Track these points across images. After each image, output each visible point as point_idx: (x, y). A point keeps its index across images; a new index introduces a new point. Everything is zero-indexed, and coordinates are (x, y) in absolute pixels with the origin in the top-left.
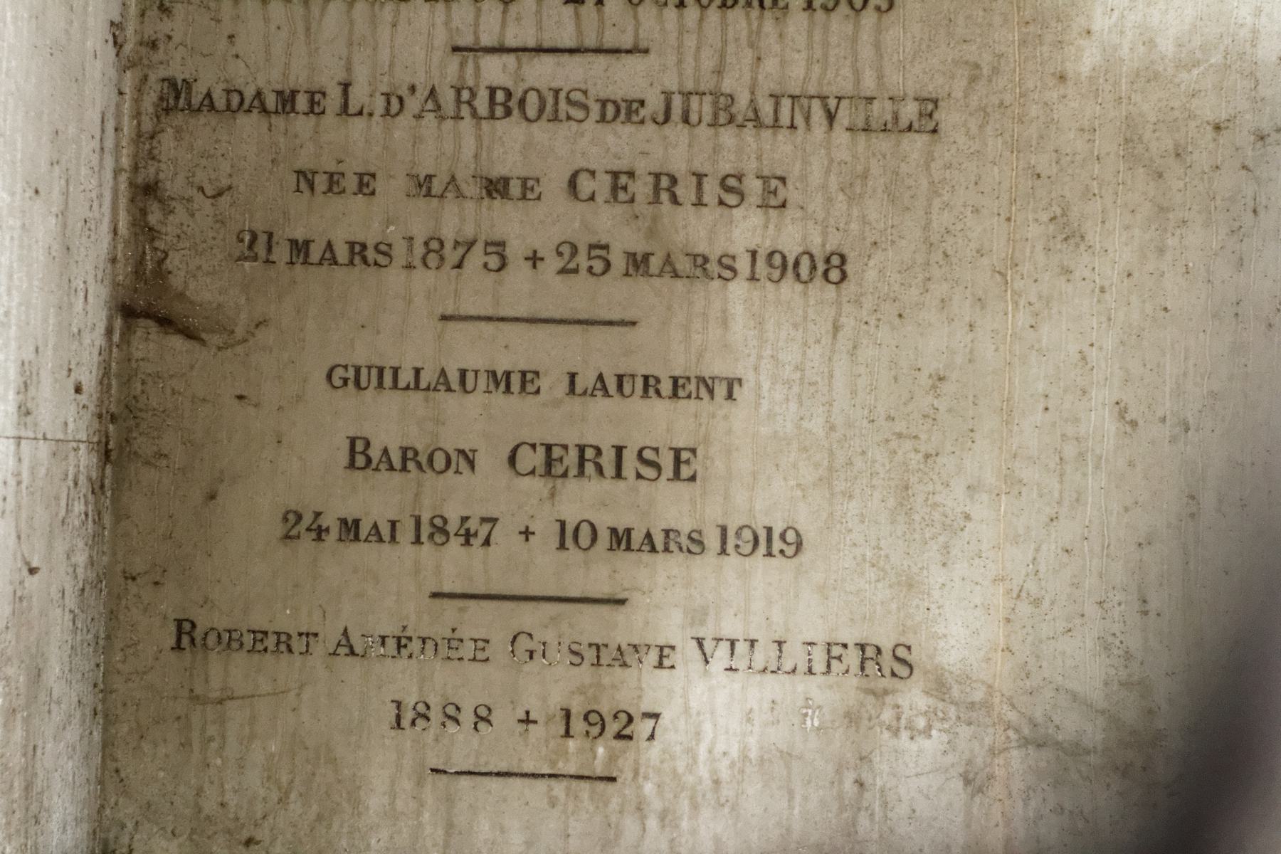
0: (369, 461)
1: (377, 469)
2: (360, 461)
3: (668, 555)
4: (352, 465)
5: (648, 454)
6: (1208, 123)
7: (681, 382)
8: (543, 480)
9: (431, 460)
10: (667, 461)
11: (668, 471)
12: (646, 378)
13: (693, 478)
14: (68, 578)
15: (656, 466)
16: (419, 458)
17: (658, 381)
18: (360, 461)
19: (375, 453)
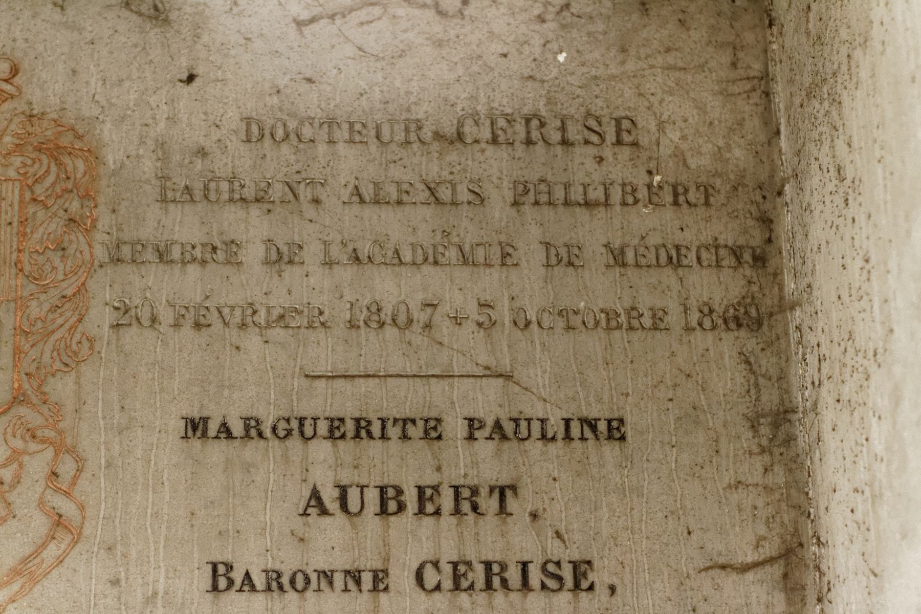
0: (231, 582)
1: (240, 590)
2: (222, 583)
3: (384, 415)
4: (215, 588)
5: (551, 568)
6: (556, 213)
7: (429, 492)
8: (484, 594)
9: (292, 582)
10: (567, 573)
11: (569, 582)
12: (382, 490)
13: (439, 438)
14: (821, 515)
15: (560, 579)
16: (506, 575)
17: (399, 492)
18: (222, 583)
19: (238, 576)
